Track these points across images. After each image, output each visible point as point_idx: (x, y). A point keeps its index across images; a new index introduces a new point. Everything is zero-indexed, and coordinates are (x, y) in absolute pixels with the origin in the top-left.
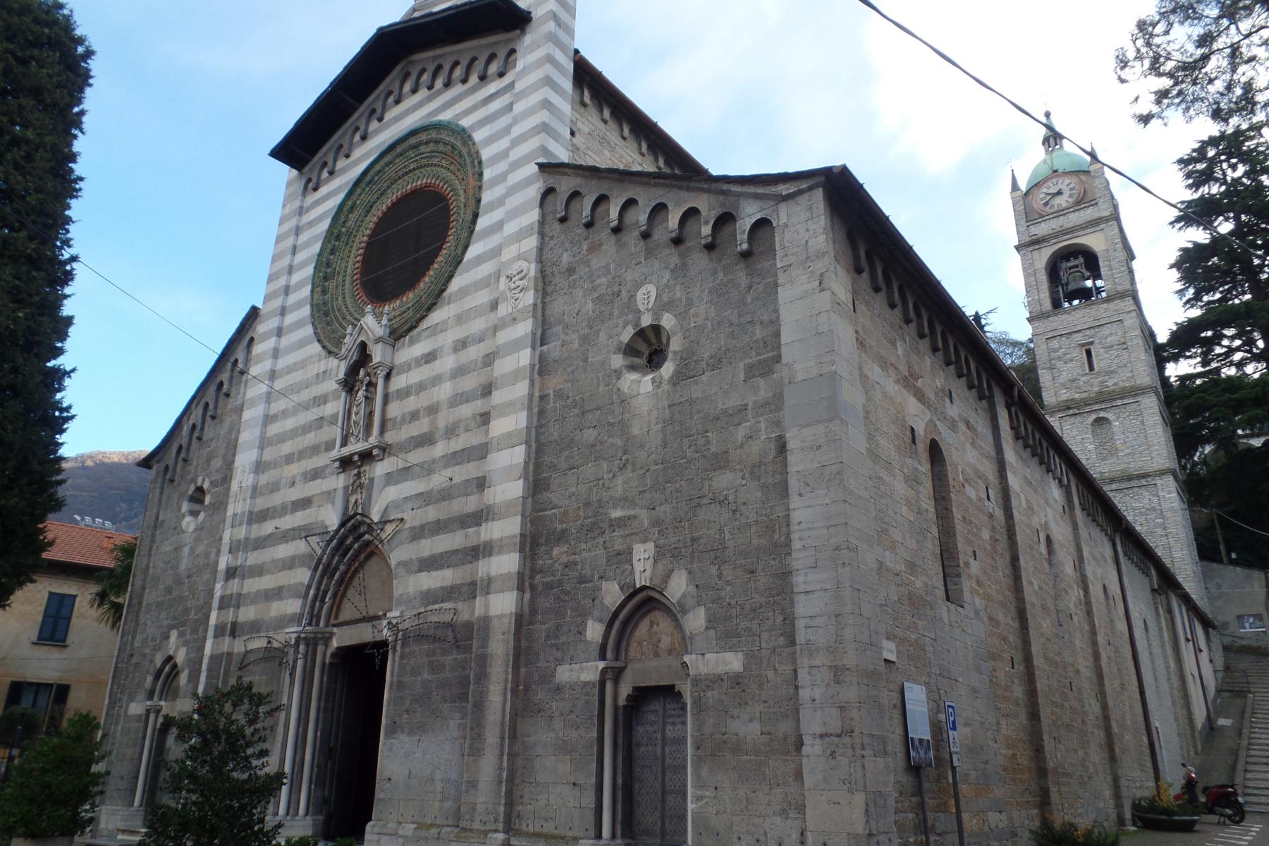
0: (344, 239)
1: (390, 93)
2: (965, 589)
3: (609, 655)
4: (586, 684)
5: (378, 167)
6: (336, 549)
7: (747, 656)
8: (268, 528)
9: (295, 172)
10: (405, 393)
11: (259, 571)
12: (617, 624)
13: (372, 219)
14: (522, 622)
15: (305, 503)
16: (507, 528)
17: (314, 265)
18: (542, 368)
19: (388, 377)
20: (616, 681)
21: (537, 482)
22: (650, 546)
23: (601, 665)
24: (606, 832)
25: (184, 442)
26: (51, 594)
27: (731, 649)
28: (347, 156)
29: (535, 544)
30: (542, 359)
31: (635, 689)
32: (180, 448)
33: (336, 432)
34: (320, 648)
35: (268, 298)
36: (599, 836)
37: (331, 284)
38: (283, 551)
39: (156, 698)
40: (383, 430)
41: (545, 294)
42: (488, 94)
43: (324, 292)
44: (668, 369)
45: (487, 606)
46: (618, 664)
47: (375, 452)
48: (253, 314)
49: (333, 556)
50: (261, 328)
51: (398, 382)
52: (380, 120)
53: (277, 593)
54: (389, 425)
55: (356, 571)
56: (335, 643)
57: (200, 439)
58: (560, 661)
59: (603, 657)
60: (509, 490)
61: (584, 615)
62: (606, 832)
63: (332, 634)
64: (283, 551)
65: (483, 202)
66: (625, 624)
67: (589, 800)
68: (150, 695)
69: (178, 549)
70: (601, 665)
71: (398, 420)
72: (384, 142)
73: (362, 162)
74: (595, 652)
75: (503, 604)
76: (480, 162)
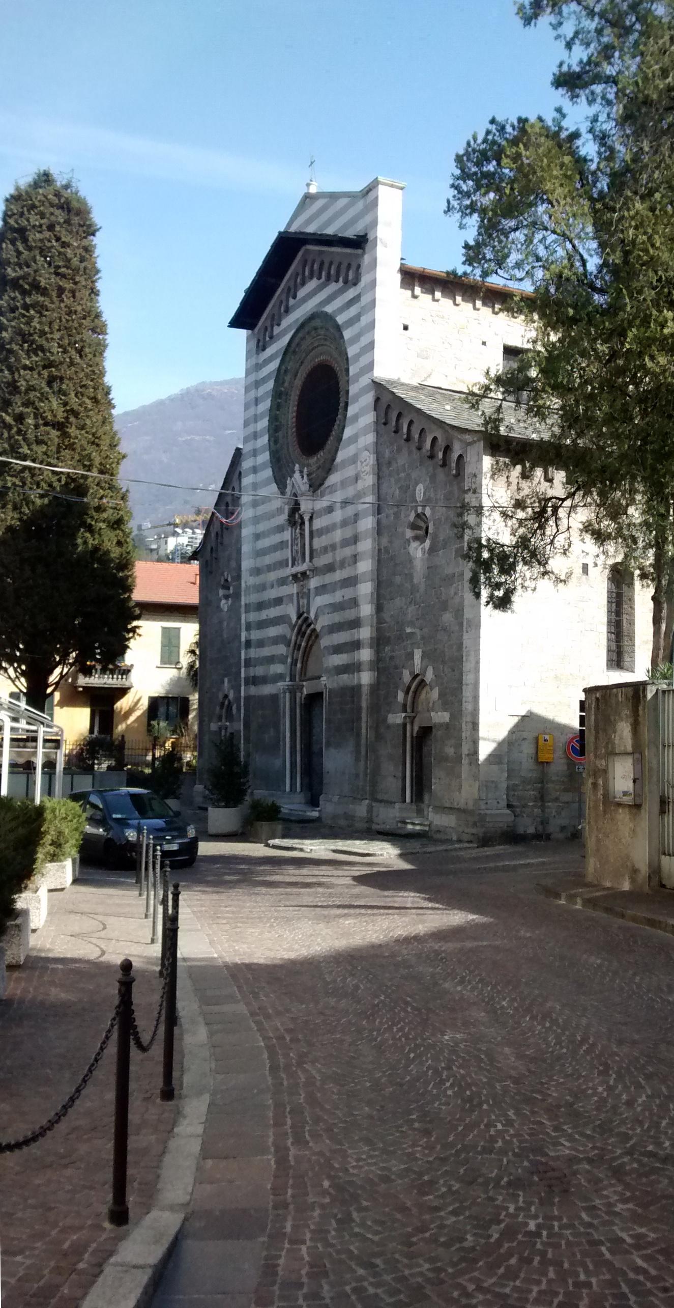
0: (284, 397)
1: (297, 274)
2: (625, 620)
3: (409, 710)
4: (398, 725)
5: (297, 340)
6: (298, 633)
7: (451, 715)
8: (265, 614)
9: (250, 332)
10: (322, 532)
11: (261, 644)
12: (411, 693)
13: (299, 382)
14: (375, 688)
15: (278, 601)
16: (365, 633)
17: (267, 418)
18: (379, 529)
19: (311, 519)
20: (412, 724)
21: (379, 608)
22: (420, 650)
23: (404, 715)
24: (408, 799)
25: (213, 544)
26: (164, 629)
27: (445, 710)
28: (279, 325)
29: (378, 645)
30: (379, 523)
31: (420, 727)
32: (212, 549)
33: (287, 554)
34: (298, 695)
35: (246, 440)
36: (405, 801)
37: (280, 434)
38: (273, 632)
39: (223, 720)
40: (311, 561)
41: (379, 478)
42: (347, 300)
43: (276, 442)
44: (427, 543)
45: (359, 678)
46: (413, 714)
47: (308, 573)
48: (238, 452)
49: (297, 637)
50: (246, 464)
51: (318, 524)
52: (295, 297)
53: (271, 660)
54: (315, 554)
55: (312, 646)
56: (305, 692)
57: (222, 544)
58: (389, 712)
59: (405, 711)
60: (366, 610)
61: (397, 688)
62: (408, 799)
63: (303, 686)
64: (273, 632)
65: (350, 394)
66: (415, 692)
67: (400, 783)
68: (220, 719)
69: (221, 622)
70: (404, 715)
71: (539, 203)
72: (298, 319)
73: (284, 335)
74: (401, 708)
75: (366, 678)
76: (347, 359)
